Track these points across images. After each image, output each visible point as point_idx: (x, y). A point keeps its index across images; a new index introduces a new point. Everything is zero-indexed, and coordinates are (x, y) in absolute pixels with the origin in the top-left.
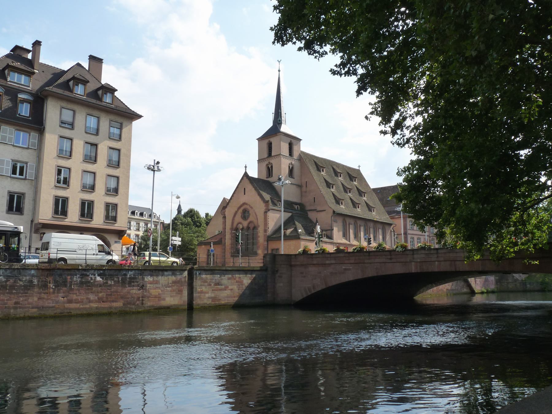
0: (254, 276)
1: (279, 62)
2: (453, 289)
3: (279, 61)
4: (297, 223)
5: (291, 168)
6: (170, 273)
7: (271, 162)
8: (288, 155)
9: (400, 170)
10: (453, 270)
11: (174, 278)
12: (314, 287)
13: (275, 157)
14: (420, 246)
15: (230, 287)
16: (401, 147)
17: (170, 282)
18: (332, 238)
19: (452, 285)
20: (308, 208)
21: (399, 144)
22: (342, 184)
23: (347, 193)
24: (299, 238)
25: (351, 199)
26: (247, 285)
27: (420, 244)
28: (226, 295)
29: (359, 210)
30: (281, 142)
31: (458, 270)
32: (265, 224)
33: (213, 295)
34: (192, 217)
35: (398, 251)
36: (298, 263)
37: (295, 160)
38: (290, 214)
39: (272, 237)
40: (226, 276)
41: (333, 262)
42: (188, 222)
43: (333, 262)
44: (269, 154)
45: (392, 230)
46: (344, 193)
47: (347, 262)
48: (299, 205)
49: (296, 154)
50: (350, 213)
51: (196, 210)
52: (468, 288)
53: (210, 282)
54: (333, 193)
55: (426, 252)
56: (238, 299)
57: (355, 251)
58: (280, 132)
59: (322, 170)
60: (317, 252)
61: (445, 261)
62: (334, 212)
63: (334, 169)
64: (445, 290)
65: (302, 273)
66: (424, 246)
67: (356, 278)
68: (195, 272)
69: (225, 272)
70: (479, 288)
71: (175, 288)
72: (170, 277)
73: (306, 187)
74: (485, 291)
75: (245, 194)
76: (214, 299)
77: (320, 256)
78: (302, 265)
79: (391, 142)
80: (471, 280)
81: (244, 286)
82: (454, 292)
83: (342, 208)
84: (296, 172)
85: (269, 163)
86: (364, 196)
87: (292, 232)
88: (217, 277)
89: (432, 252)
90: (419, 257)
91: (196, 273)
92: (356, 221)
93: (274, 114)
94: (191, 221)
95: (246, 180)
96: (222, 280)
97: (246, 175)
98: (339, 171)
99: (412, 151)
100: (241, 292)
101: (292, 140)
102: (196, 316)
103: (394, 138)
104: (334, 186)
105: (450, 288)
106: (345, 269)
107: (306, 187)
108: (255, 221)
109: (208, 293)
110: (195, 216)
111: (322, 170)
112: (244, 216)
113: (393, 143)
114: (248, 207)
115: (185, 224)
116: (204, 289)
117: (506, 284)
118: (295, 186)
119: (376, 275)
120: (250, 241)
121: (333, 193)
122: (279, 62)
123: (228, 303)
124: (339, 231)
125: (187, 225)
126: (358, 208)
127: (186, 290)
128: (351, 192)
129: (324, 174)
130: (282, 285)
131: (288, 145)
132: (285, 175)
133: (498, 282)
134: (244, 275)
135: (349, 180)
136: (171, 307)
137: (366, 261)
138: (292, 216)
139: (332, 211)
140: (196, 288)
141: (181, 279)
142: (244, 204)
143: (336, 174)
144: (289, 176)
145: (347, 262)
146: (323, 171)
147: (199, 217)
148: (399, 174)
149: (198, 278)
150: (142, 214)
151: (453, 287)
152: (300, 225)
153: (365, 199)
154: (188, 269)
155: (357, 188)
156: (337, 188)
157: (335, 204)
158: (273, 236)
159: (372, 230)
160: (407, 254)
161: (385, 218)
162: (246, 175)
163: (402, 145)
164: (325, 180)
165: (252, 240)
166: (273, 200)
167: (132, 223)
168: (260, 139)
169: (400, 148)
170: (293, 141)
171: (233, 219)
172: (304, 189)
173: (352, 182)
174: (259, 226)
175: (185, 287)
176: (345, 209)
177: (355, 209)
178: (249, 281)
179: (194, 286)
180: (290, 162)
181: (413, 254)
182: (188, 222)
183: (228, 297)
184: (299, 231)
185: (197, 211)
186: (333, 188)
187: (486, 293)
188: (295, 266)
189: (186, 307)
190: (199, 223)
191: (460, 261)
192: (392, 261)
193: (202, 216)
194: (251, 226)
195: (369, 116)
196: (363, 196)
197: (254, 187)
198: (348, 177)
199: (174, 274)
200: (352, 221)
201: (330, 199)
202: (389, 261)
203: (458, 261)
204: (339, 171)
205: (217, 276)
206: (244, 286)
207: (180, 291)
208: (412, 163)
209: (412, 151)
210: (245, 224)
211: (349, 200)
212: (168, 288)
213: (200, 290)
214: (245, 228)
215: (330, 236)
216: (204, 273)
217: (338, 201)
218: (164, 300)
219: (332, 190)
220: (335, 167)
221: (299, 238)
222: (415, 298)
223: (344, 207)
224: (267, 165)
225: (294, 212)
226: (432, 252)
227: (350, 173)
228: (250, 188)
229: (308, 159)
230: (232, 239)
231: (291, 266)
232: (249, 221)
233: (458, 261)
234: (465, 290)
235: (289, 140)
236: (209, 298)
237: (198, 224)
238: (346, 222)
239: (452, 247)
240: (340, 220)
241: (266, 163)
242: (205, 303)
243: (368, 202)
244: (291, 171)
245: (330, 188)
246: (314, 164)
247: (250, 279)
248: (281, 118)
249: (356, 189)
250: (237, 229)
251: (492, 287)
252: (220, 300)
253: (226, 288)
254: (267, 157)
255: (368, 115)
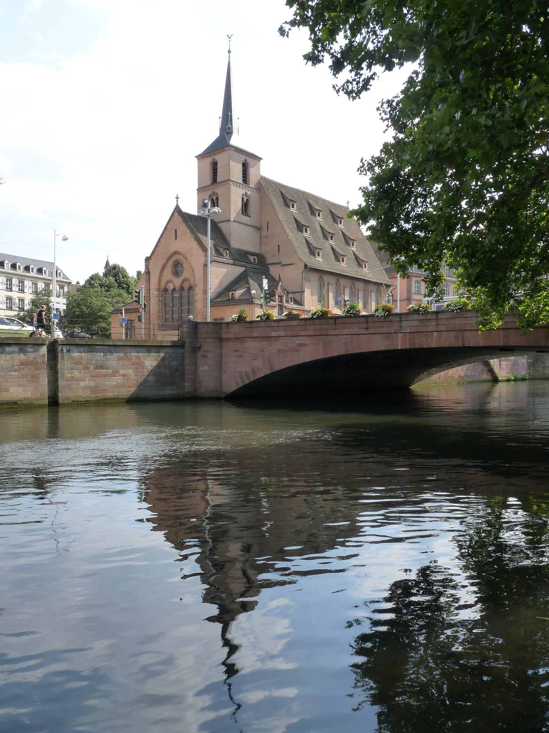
0: (162, 355)
1: (230, 38)
2: (468, 376)
3: (229, 36)
4: (251, 281)
5: (245, 200)
6: (16, 349)
7: (216, 191)
8: (240, 180)
9: (366, 163)
10: (460, 344)
11: (22, 357)
12: (254, 372)
13: (222, 184)
14: (412, 308)
15: (122, 372)
16: (354, 98)
17: (16, 362)
18: (302, 304)
19: (467, 370)
20: (269, 261)
21: (349, 93)
22: (321, 227)
23: (327, 239)
24: (252, 303)
25: (332, 248)
26: (150, 368)
27: (411, 306)
28: (115, 383)
29: (343, 264)
30: (231, 161)
31: (467, 345)
32: (204, 282)
33: (92, 384)
34: (115, 275)
35: (378, 316)
36: (231, 336)
37: (252, 190)
38: (243, 269)
39: (215, 301)
40: (115, 355)
41: (282, 333)
42: (109, 283)
43: (282, 333)
44: (214, 179)
45: (391, 294)
46: (322, 240)
47: (302, 333)
48: (257, 256)
49: (253, 180)
50: (329, 268)
51: (121, 266)
52: (489, 373)
53: (87, 363)
54: (306, 239)
55: (421, 317)
56: (136, 390)
57: (315, 317)
58: (229, 146)
59: (291, 206)
60: (259, 319)
61: (448, 331)
62: (306, 266)
63: (309, 205)
64: (456, 376)
65: (237, 351)
66: (417, 307)
67: (315, 358)
68: (59, 348)
69: (112, 349)
70: (505, 375)
71: (25, 371)
72: (16, 356)
73: (268, 230)
74: (513, 378)
75: (176, 239)
76: (93, 390)
77: (263, 324)
78: (237, 339)
79: (334, 87)
80: (494, 362)
81: (145, 370)
82: (470, 380)
83: (319, 261)
84: (253, 208)
85: (214, 193)
86: (353, 245)
87: (242, 295)
88: (99, 356)
89: (429, 317)
90: (408, 325)
91: (62, 350)
92: (338, 280)
93: (221, 119)
94: (114, 281)
95: (177, 217)
96: (107, 360)
97: (177, 210)
98: (317, 208)
99: (387, 126)
100: (141, 379)
101: (247, 158)
102: (64, 416)
103: (337, 76)
104: (308, 230)
105: (464, 373)
106: (301, 345)
107: (268, 230)
108: (191, 278)
109: (84, 380)
110: (120, 275)
111: (291, 206)
112: (176, 270)
113: (337, 88)
114: (181, 258)
115: (106, 286)
116: (76, 374)
117: (541, 368)
118: (251, 228)
119: (344, 353)
120: (185, 308)
121: (306, 239)
122: (230, 38)
123: (118, 395)
124: (312, 294)
125: (108, 287)
126: (343, 261)
127: (46, 375)
128: (333, 238)
129: (294, 211)
130: (206, 368)
131: (241, 166)
132: (237, 211)
133: (532, 365)
134: (146, 354)
135: (332, 221)
136: (19, 403)
137: (331, 332)
138: (245, 271)
139: (303, 266)
140: (63, 373)
141: (35, 358)
142: (176, 253)
143: (313, 211)
144: (243, 214)
145: (302, 333)
146: (293, 206)
147: (125, 276)
148: (361, 170)
149: (66, 357)
150: (14, 266)
151: (469, 373)
152: (257, 285)
153: (354, 249)
154: (47, 343)
155: (343, 233)
156: (313, 232)
157: (308, 254)
158: (216, 300)
159: (361, 294)
160: (392, 321)
161: (383, 278)
162: (177, 210)
163: (354, 95)
164: (295, 219)
165: (187, 306)
166: (218, 248)
167: (14, 280)
168: (200, 157)
169: (351, 99)
170: (250, 161)
171: (161, 276)
172: (264, 232)
173: (335, 225)
174: (196, 285)
175: (42, 371)
176: (324, 263)
177: (338, 263)
178: (155, 363)
179: (59, 370)
180: (243, 191)
181: (400, 321)
182: (109, 283)
183: (118, 386)
184: (253, 292)
185: (122, 268)
186: (306, 232)
187: (513, 380)
188: (227, 339)
189: (46, 402)
190: (126, 284)
191: (470, 330)
192: (370, 331)
193: (130, 275)
194: (186, 286)
195: (287, 27)
196: (351, 244)
197: (189, 227)
198: (330, 217)
199: (22, 351)
200: (333, 280)
201: (300, 248)
202: (364, 331)
203: (468, 330)
204: (317, 207)
205: (99, 354)
206: (145, 370)
207: (35, 378)
208: (386, 148)
209: (387, 126)
210: (177, 282)
211: (329, 249)
212: (13, 373)
213: (69, 375)
214: (177, 288)
215: (299, 300)
216: (76, 350)
217: (313, 251)
218: (7, 390)
219: (305, 235)
220: (311, 202)
221: (252, 303)
222: (412, 387)
223: (321, 260)
224: (210, 196)
225: (248, 265)
226: (429, 317)
227: (334, 211)
228: (183, 228)
229: (271, 188)
230: (159, 305)
231: (221, 340)
232: (182, 277)
233: (468, 330)
234: (486, 376)
235: (243, 158)
236: (85, 387)
237: (124, 286)
238: (323, 281)
239: (459, 309)
240: (315, 277)
241: (210, 192)
242: (78, 396)
243: (357, 253)
244: (245, 206)
245: (302, 232)
246: (281, 196)
247: (155, 360)
248: (232, 125)
249: (341, 234)
250: (166, 290)
251: (523, 372)
252: (105, 390)
253: (115, 373)
254: (210, 185)
255: (284, 26)
